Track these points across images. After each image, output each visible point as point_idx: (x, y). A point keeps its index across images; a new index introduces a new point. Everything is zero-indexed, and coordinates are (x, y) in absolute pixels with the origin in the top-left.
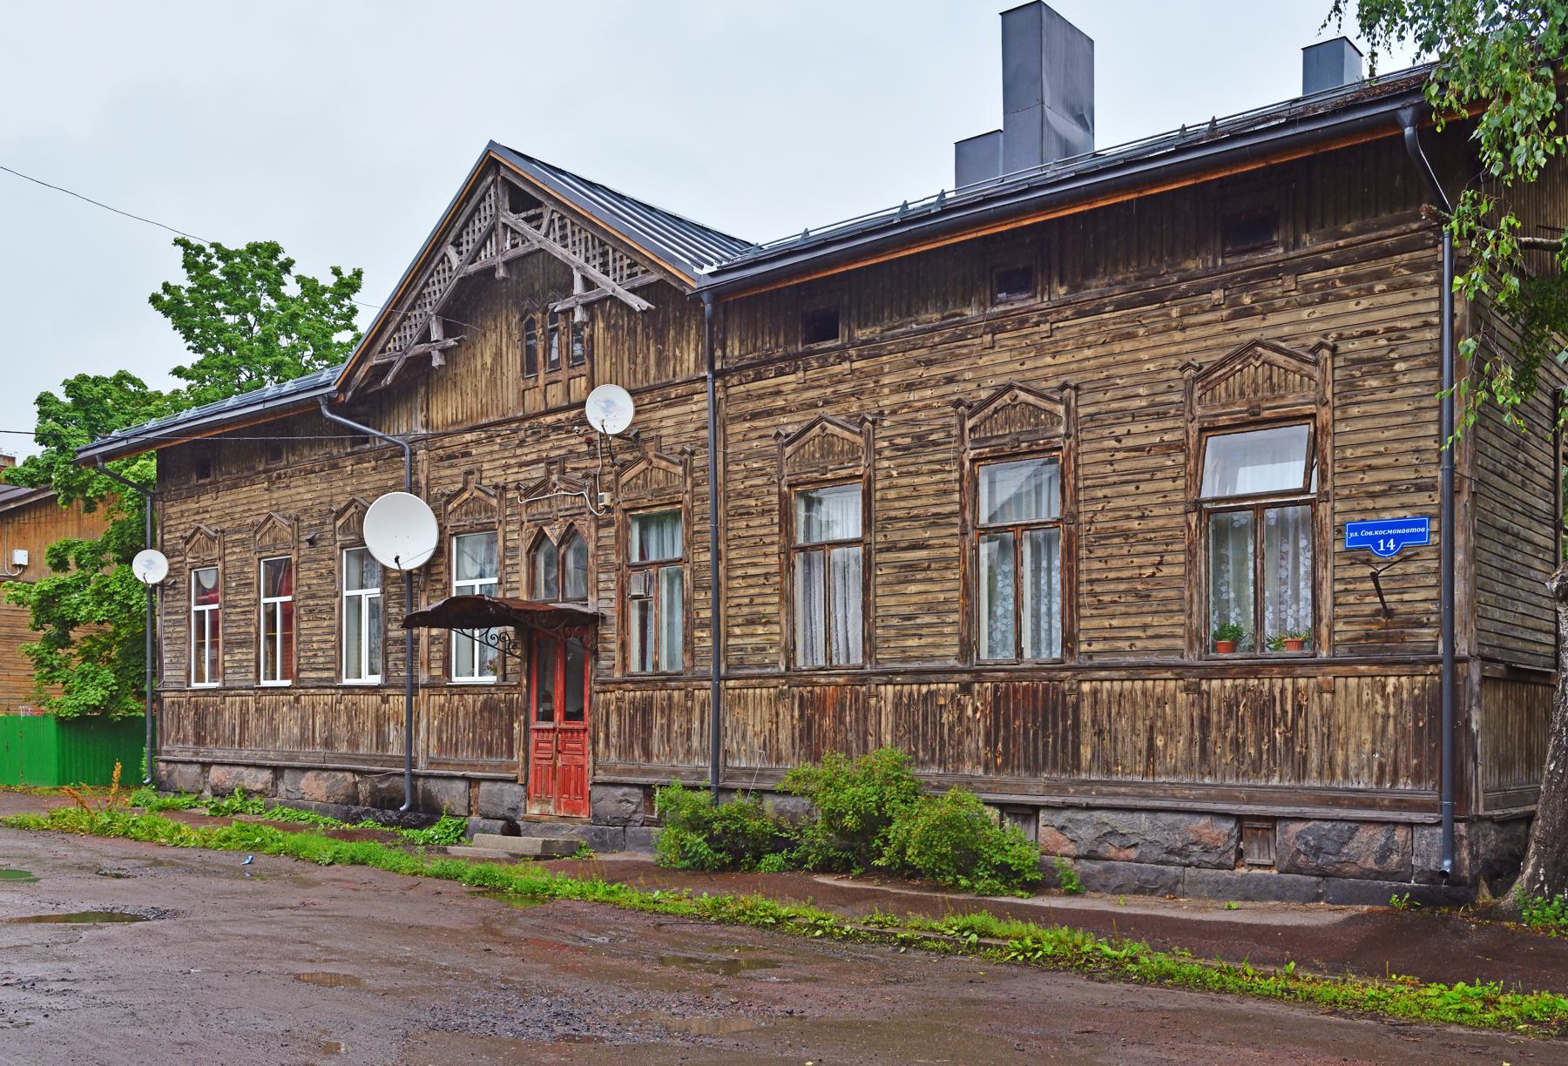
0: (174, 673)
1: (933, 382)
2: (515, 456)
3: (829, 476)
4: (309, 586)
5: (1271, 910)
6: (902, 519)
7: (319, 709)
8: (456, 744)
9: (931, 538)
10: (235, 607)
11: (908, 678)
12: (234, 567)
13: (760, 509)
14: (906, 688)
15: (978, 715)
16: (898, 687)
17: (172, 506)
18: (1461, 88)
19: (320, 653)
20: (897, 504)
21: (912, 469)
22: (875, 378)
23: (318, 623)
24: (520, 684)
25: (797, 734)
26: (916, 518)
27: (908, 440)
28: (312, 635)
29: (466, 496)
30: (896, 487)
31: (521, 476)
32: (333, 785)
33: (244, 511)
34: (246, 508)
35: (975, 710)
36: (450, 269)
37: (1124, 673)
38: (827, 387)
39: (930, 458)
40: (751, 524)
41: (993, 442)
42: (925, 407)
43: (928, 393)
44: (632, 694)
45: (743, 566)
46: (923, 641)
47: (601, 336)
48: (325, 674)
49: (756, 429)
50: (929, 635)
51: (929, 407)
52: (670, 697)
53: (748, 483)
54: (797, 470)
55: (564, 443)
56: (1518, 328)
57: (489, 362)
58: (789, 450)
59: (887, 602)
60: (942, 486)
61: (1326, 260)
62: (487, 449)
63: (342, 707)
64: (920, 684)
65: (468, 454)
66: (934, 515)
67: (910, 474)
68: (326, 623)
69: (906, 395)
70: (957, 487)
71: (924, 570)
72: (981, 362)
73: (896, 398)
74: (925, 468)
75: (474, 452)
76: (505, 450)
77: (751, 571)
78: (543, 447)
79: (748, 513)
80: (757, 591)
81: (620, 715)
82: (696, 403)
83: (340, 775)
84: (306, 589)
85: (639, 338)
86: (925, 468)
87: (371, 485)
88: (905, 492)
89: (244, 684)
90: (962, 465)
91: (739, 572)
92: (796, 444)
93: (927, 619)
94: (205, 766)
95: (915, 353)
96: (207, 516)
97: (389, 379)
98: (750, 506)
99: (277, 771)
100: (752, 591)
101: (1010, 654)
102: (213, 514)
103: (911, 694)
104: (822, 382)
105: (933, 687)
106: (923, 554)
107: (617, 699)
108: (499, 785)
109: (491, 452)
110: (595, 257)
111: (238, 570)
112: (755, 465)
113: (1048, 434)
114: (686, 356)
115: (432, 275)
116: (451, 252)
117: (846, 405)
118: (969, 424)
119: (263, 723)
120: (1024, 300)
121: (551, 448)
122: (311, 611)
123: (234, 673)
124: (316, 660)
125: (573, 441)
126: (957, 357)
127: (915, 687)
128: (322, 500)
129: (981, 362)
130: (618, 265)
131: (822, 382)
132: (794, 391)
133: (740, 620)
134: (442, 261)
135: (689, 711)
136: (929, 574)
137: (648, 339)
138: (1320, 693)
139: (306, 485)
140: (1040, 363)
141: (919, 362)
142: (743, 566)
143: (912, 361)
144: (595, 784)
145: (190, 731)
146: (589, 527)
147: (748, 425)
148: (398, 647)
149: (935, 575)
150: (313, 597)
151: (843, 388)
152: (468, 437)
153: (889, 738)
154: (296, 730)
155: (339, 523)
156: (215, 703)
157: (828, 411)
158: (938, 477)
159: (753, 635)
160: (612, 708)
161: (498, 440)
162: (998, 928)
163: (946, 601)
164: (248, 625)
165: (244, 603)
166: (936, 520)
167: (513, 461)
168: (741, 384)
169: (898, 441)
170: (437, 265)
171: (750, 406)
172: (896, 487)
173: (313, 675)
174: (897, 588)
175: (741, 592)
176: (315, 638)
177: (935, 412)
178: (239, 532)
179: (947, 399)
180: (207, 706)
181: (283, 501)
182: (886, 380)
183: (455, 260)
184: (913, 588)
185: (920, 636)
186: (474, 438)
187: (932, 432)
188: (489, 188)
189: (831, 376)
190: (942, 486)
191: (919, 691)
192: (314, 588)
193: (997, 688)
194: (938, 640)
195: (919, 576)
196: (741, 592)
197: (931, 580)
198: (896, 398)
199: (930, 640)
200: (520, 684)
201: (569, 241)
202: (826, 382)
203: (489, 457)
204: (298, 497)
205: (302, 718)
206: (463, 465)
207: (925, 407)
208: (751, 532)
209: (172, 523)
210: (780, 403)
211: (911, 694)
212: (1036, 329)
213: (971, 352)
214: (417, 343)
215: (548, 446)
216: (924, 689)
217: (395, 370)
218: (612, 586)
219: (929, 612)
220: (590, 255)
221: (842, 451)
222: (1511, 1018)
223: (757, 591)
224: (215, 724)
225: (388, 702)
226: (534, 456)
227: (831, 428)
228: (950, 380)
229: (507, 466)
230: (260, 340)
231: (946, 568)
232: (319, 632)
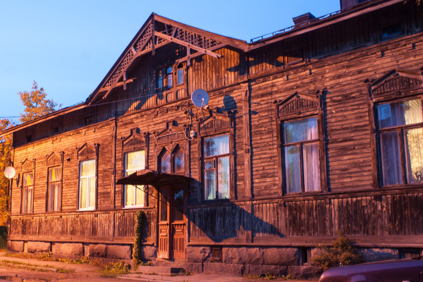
0: (15, 209)
1: (351, 74)
2: (153, 121)
3: (301, 115)
4: (67, 176)
5: (58, 199)
6: (338, 130)
7: (69, 220)
8: (126, 232)
9: (354, 136)
10: (38, 185)
11: (346, 195)
12: (38, 171)
13: (267, 132)
14: (345, 200)
15: (384, 209)
16: (340, 200)
17: (17, 152)
18: (7, 142)
19: (70, 200)
20: (336, 124)
21: (343, 109)
22: (321, 75)
23: (70, 189)
24: (154, 207)
25: (288, 222)
26: (346, 128)
27: (340, 98)
28: (67, 193)
29: (132, 138)
30: (335, 117)
31: (155, 129)
32: (74, 248)
33: (43, 152)
34: (44, 150)
35: (382, 207)
36: (132, 55)
37: (334, 196)
38: (298, 81)
39: (352, 104)
40: (262, 137)
41: (386, 94)
42: (348, 84)
43: (349, 78)
44: (206, 209)
45: (259, 155)
46: (353, 179)
47: (191, 74)
48: (72, 207)
49: (263, 100)
50: (355, 177)
51: (350, 84)
52: (224, 209)
53: (260, 122)
54: (285, 114)
55: (174, 115)
56: (109, 148)
57: (142, 89)
58: (281, 107)
59: (333, 164)
60: (359, 114)
61: (396, 222)
62: (141, 120)
63: (78, 219)
64: (352, 198)
65: (133, 123)
66: (355, 127)
67: (341, 111)
68: (72, 189)
69: (338, 80)
70: (367, 114)
71: (352, 149)
72: (376, 64)
73: (333, 82)
74: (350, 108)
75: (135, 122)
76: (148, 119)
77: (263, 156)
78: (165, 117)
79: (261, 134)
80: (266, 164)
81: (200, 218)
82: (235, 94)
83: (77, 244)
84: (66, 177)
85: (208, 72)
86: (350, 108)
87: (92, 138)
88: (340, 119)
89: (40, 212)
90: (369, 105)
91: (257, 157)
92: (284, 104)
93: (354, 170)
94: (25, 242)
95: (342, 63)
96: (30, 154)
97: (106, 96)
98: (262, 131)
99: (52, 243)
100: (264, 164)
101: (402, 183)
102: (32, 154)
103: (347, 202)
104: (295, 79)
105: (359, 198)
106: (351, 143)
107: (199, 211)
108: (115, 246)
109: (142, 121)
110: (196, 42)
111: (40, 172)
112: (264, 115)
113: (415, 88)
114: (230, 76)
115: (125, 58)
116: (133, 50)
117: (308, 87)
118: (373, 88)
119: (48, 226)
120: (297, 220)
121: (169, 117)
122: (67, 185)
123: (37, 208)
124: (68, 202)
125: (178, 113)
126: (363, 63)
127: (349, 199)
128: (73, 145)
129: (376, 64)
130: (206, 43)
131: (295, 79)
132: (282, 84)
133: (258, 176)
134: (129, 52)
135: (234, 214)
136: (354, 151)
137: (212, 72)
138: (307, 105)
139: (66, 140)
140: (407, 60)
141: (344, 67)
142: (259, 155)
143: (340, 66)
144: (189, 246)
145: (20, 229)
146: (186, 145)
147: (259, 99)
148: (102, 196)
149: (357, 151)
150: (68, 179)
151: (306, 81)
152: (133, 116)
153: (337, 221)
154: (60, 228)
155: (80, 152)
156: (29, 220)
157: (299, 90)
158: (357, 111)
159: (264, 182)
160: (197, 215)
161: (145, 116)
162: (71, 181)
163: (364, 162)
164: (43, 191)
165: (42, 184)
166: (356, 129)
167: (152, 123)
168: (256, 84)
169: (335, 98)
170: (127, 54)
171: (261, 92)
172: (335, 117)
173: (67, 208)
174: (338, 158)
175: (259, 165)
176: (68, 194)
177: (353, 85)
178: (41, 159)
179: (359, 80)
180: (26, 220)
181: (58, 147)
182: (327, 75)
183: (134, 52)
184: (346, 158)
185: (351, 177)
186: (135, 117)
187: (352, 93)
188: (150, 24)
189: (299, 77)
190: (359, 114)
191: (352, 201)
192: (68, 176)
193: (393, 198)
194: (360, 178)
195: (349, 152)
196: (259, 165)
197: (356, 154)
198: (333, 82)
199: (356, 179)
200: (154, 207)
201: (184, 38)
202: (297, 79)
203: (141, 123)
204: (63, 145)
205: (63, 224)
206: (130, 127)
207: (348, 84)
208: (262, 141)
209: (17, 158)
210: (275, 89)
211: (347, 202)
212: (405, 47)
213: (370, 60)
214: (117, 83)
215: (167, 116)
216: (354, 199)
217: (108, 93)
218: (196, 167)
219: (355, 167)
220: (194, 41)
221: (307, 105)
222: (132, 130)
223: (266, 164)
224: (30, 227)
225: (97, 216)
226: (161, 121)
227: (302, 97)
228: (360, 72)
229: (149, 125)
230: (207, 126)
231: (363, 148)
232: (70, 192)
